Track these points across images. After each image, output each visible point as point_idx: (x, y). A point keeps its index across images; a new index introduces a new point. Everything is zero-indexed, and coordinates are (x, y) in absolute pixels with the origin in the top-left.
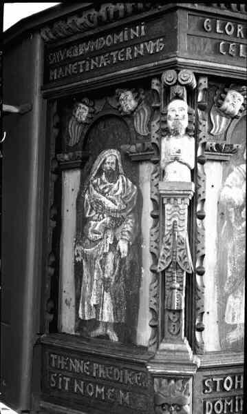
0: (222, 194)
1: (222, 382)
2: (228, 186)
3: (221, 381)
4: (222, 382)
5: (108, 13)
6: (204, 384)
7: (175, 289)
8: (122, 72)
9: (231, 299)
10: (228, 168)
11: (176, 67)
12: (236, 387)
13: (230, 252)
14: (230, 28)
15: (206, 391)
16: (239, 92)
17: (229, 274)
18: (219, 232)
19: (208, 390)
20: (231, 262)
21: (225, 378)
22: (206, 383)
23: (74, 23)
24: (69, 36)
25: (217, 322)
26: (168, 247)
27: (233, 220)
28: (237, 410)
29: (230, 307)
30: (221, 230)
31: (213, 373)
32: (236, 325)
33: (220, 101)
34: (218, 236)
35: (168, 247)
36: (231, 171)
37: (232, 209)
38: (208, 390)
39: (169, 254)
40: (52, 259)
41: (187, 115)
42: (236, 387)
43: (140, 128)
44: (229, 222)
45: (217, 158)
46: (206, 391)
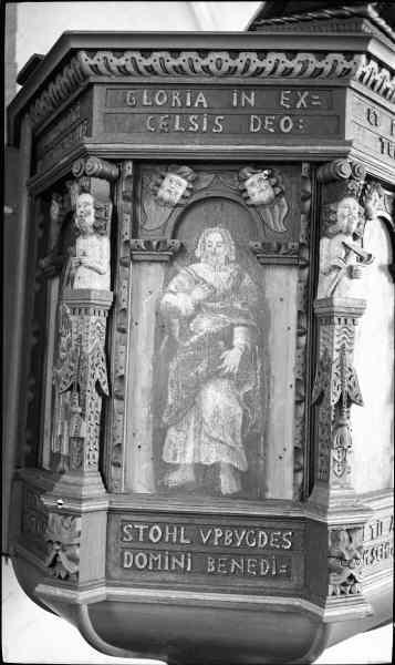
0: (163, 302)
1: (146, 532)
2: (171, 292)
3: (144, 530)
4: (146, 532)
5: (247, 66)
6: (122, 531)
7: (74, 413)
8: (188, 147)
9: (172, 432)
10: (172, 269)
11: (85, 154)
12: (167, 539)
13: (172, 375)
14: (160, 98)
15: (125, 539)
16: (180, 174)
17: (170, 401)
18: (157, 347)
19: (127, 537)
20: (172, 386)
21: (150, 527)
22: (125, 530)
23: (305, 64)
24: (43, 122)
25: (153, 459)
26: (72, 365)
27: (177, 334)
28: (167, 568)
29: (171, 442)
30: (160, 344)
31: (134, 518)
32: (178, 465)
33: (156, 188)
34: (155, 354)
35: (72, 365)
36: (176, 273)
37: (176, 321)
38: (127, 537)
39: (72, 373)
40: (32, 382)
41: (93, 211)
42: (167, 539)
43: (274, 218)
44: (171, 336)
45: (156, 258)
46: (125, 539)
